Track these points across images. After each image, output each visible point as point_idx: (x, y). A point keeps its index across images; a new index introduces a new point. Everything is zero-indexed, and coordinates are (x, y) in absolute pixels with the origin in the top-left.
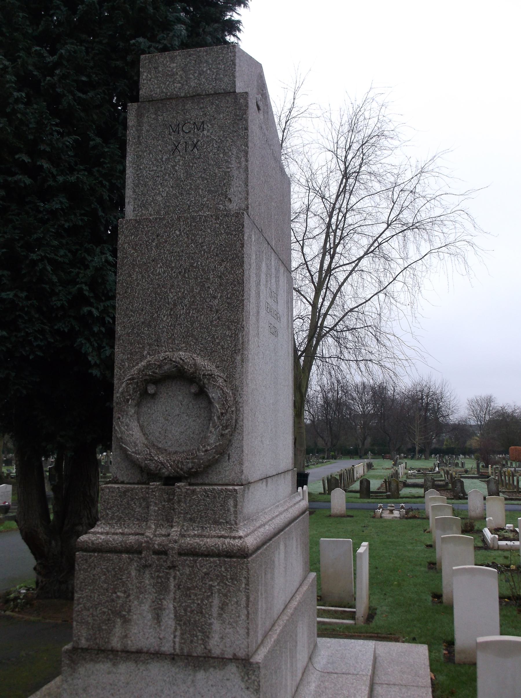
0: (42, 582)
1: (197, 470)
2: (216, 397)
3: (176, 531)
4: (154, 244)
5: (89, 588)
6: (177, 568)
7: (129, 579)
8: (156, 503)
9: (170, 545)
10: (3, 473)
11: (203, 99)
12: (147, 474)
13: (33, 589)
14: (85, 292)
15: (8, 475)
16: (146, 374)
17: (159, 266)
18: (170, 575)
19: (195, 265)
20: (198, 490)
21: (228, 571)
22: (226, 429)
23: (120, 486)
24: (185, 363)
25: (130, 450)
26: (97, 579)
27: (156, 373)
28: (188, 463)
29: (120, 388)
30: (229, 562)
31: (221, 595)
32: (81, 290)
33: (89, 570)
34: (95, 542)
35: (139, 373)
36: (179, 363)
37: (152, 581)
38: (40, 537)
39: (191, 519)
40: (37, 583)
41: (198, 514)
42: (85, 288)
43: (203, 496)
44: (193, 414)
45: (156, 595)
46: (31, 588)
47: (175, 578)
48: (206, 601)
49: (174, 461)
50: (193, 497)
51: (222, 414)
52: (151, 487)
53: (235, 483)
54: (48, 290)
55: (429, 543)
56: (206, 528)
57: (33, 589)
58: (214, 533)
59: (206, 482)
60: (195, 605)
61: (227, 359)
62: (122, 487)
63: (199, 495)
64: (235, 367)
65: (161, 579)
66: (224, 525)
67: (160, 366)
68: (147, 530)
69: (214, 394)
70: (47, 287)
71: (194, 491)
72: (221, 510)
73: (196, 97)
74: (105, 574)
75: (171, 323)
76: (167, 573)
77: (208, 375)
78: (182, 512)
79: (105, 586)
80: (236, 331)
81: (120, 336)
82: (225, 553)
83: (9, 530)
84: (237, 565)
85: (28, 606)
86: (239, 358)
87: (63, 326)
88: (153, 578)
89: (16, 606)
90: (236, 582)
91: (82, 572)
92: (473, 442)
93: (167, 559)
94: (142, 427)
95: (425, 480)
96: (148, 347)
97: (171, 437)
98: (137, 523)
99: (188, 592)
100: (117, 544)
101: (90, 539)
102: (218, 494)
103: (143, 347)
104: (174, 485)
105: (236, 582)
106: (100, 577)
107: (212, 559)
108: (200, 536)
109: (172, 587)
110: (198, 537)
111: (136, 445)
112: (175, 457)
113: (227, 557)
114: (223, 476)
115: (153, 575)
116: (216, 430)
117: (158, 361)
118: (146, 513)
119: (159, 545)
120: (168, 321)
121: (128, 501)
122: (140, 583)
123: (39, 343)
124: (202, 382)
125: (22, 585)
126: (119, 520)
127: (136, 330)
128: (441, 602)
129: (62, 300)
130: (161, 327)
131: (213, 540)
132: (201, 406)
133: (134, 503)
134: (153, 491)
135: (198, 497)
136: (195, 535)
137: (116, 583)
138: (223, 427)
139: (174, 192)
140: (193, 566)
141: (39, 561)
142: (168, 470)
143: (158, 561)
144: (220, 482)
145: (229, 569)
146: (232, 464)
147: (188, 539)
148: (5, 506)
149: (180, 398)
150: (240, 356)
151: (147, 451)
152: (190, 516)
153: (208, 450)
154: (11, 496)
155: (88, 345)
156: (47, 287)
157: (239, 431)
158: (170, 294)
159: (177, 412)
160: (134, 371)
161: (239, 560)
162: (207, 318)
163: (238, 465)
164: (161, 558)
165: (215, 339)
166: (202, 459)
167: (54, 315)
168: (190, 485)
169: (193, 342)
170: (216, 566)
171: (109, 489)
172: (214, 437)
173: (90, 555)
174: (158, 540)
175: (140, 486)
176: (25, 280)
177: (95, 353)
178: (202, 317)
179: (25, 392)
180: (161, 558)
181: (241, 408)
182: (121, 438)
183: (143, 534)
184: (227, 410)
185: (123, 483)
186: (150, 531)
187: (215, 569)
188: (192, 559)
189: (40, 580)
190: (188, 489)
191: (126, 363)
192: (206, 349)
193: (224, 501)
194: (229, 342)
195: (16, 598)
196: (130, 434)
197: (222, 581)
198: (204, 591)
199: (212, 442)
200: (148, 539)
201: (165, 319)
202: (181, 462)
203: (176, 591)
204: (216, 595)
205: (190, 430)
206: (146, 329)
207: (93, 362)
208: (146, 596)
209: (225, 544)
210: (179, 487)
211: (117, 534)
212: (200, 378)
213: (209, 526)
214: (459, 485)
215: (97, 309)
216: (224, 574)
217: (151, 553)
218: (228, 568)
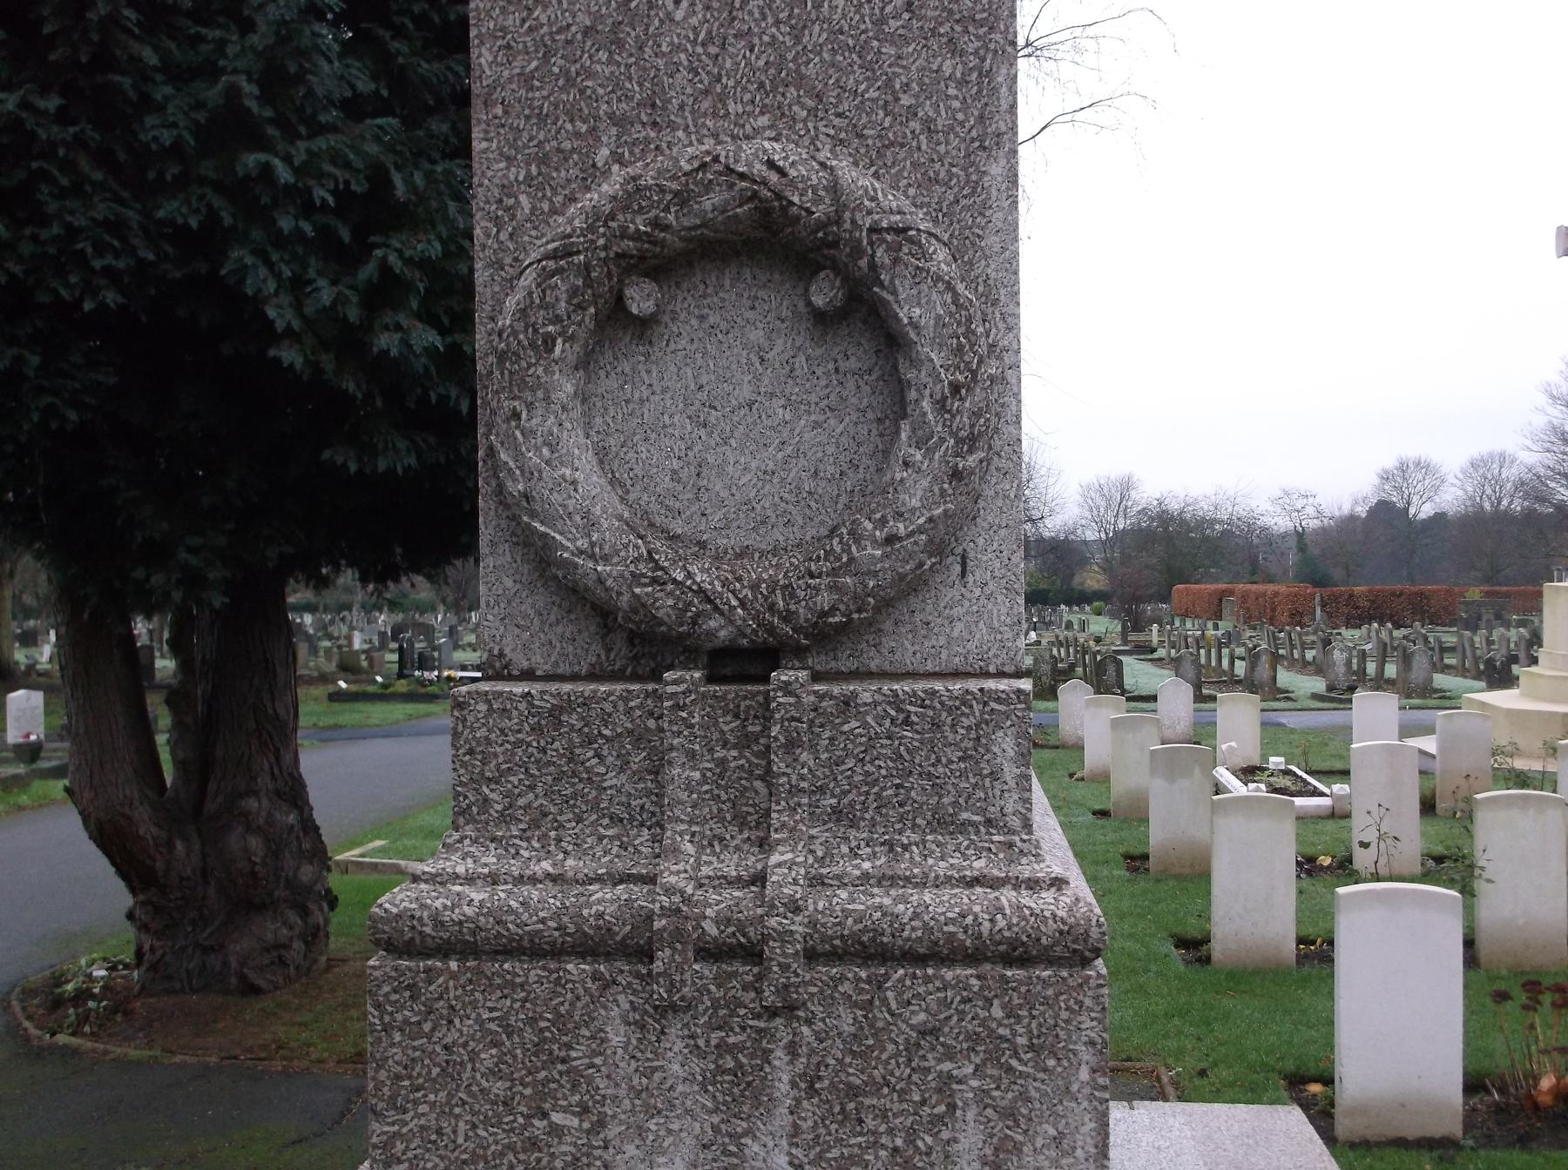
0: (152, 949)
1: (850, 620)
2: (927, 322)
3: (791, 865)
5: (432, 1097)
6: (801, 1013)
7: (598, 1061)
8: (692, 755)
9: (773, 922)
10: (17, 663)
12: (638, 641)
13: (126, 966)
14: (247, 103)
15: (31, 668)
16: (624, 229)
18: (773, 1039)
20: (866, 697)
21: (1019, 1018)
22: (970, 452)
23: (535, 688)
24: (792, 183)
25: (568, 543)
26: (462, 1063)
27: (666, 228)
28: (817, 589)
29: (503, 300)
30: (1020, 983)
31: (989, 1111)
32: (233, 93)
33: (427, 1027)
34: (447, 916)
35: (591, 228)
36: (764, 183)
37: (696, 1065)
38: (141, 832)
39: (837, 812)
40: (139, 954)
41: (867, 793)
42: (249, 88)
43: (887, 723)
44: (813, 398)
45: (716, 1119)
46: (120, 962)
47: (792, 1050)
48: (929, 1139)
49: (755, 587)
50: (846, 728)
51: (956, 388)
52: (670, 689)
53: (992, 669)
54: (131, 94)
55: (1097, 807)
56: (905, 848)
57: (126, 966)
58: (942, 868)
59: (873, 666)
60: (883, 1153)
61: (951, 175)
62: (543, 692)
63: (869, 719)
64: (985, 205)
65: (736, 1059)
66: (977, 833)
67: (683, 199)
68: (663, 865)
69: (916, 308)
70: (126, 82)
71: (847, 703)
72: (963, 774)
74: (496, 1044)
75: (709, 32)
76: (759, 1031)
77: (889, 229)
78: (804, 784)
79: (499, 1088)
80: (983, 60)
81: (492, 88)
82: (1002, 948)
83: (43, 804)
84: (1057, 995)
85: (119, 1017)
86: (996, 169)
87: (184, 210)
88: (703, 1055)
89: (84, 1019)
90: (1051, 1063)
91: (397, 1037)
92: (1093, 580)
93: (760, 978)
94: (602, 456)
95: (1036, 660)
96: (614, 131)
97: (724, 494)
98: (610, 832)
99: (852, 1105)
100: (543, 921)
101: (423, 906)
102: (950, 710)
103: (593, 130)
104: (765, 679)
105: (1051, 1063)
106: (474, 1056)
107: (949, 975)
108: (888, 880)
109: (784, 1087)
110: (879, 884)
111: (591, 524)
112: (753, 571)
113: (1009, 961)
114: (942, 641)
115: (701, 1043)
116: (930, 452)
117: (674, 178)
118: (649, 793)
119: (723, 921)
120: (694, 21)
121: (570, 749)
122: (649, 1073)
123: (109, 260)
124: (863, 263)
125: (95, 955)
126: (535, 824)
127: (557, 64)
128: (1207, 960)
129: (174, 125)
130: (664, 48)
131: (946, 893)
132: (843, 365)
133: (598, 755)
134: (678, 707)
135: (865, 725)
136: (866, 876)
137: (543, 1074)
138: (959, 441)
140: (871, 1002)
141: (141, 897)
142: (731, 622)
143: (719, 986)
144: (929, 667)
145: (1024, 1013)
146: (978, 592)
147: (844, 894)
148: (30, 745)
149: (756, 335)
150: (1003, 162)
151: (637, 547)
152: (834, 801)
153: (900, 539)
154: (42, 719)
155: (263, 272)
156: (126, 82)
157: (1003, 463)
159: (746, 393)
160: (572, 219)
161: (1065, 974)
164: (735, 974)
165: (894, 92)
166: (875, 574)
167: (151, 175)
168: (816, 677)
169: (803, 107)
170: (965, 1001)
171: (488, 702)
172: (925, 483)
173: (428, 970)
174: (717, 902)
175: (619, 687)
176: (52, 57)
177: (285, 299)
179: (73, 416)
180: (735, 974)
182: (527, 497)
183: (650, 880)
184: (974, 373)
185: (528, 675)
186: (681, 867)
187: (961, 1014)
188: (863, 974)
189: (147, 947)
190: (821, 697)
191: (523, 198)
192: (860, 136)
193: (978, 739)
194: (956, 104)
195: (81, 996)
196: (563, 477)
197: (993, 1057)
198: (917, 1098)
199: (915, 503)
200: (677, 899)
201: (679, 15)
202: (785, 587)
203: (798, 1101)
204: (971, 1115)
205: (802, 462)
206: (603, 56)
207: (280, 325)
208: (675, 1127)
209: (1001, 910)
210: (786, 688)
211: (534, 880)
212: (859, 241)
213: (915, 837)
214: (1111, 670)
215: (287, 159)
216: (1001, 1031)
217: (691, 955)
218: (1020, 1007)
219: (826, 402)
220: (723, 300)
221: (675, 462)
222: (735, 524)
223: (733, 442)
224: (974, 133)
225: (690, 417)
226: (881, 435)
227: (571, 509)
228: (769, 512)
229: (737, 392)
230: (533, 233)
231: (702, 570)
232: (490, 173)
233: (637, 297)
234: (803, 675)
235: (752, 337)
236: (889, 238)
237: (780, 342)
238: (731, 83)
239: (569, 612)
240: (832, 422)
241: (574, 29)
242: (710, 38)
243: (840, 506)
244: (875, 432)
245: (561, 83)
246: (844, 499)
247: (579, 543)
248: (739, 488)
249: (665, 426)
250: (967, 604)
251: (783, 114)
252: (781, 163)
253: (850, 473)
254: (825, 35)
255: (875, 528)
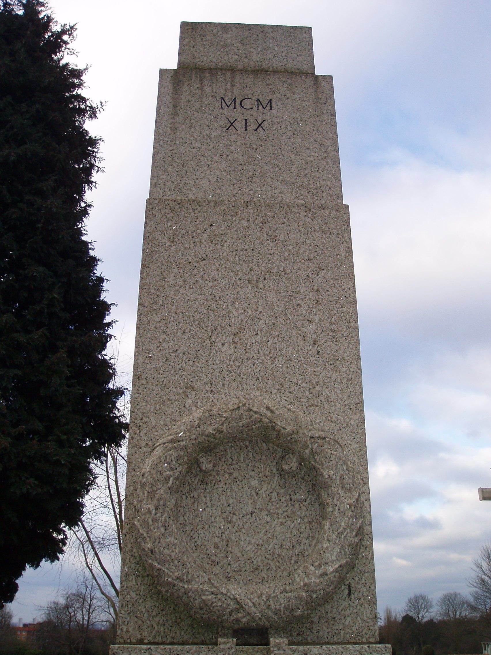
4: (205, 236)
11: (269, 75)
17: (214, 267)
19: (275, 270)
44: (280, 512)
73: (260, 72)
97: (239, 555)
132: (293, 497)
139: (228, 176)
149: (254, 483)
151: (203, 577)
158: (234, 311)
159: (250, 508)
162: (298, 351)
163: (367, 606)
178: (290, 349)
181: (366, 503)
191: (152, 419)
202: (274, 597)
205: (275, 541)
206: (191, 363)
219: (286, 513)
220: (240, 466)
221: (216, 538)
222: (244, 569)
223: (243, 530)
224: (346, 403)
225: (224, 519)
226: (311, 529)
227: (173, 557)
228: (260, 564)
229: (245, 508)
230: (156, 433)
231: (234, 589)
232: (138, 407)
233: (205, 462)
234: (286, 641)
235: (253, 484)
236: (319, 441)
237: (265, 486)
238: (245, 377)
239: (162, 610)
240: (289, 522)
241: (179, 352)
242: (236, 359)
243: (293, 562)
244: (308, 528)
245: (172, 372)
246: (294, 558)
247: (176, 574)
248: (246, 552)
249: (212, 522)
250: (351, 608)
251: (267, 391)
252: (272, 408)
253: (297, 546)
254: (284, 361)
255: (316, 569)
